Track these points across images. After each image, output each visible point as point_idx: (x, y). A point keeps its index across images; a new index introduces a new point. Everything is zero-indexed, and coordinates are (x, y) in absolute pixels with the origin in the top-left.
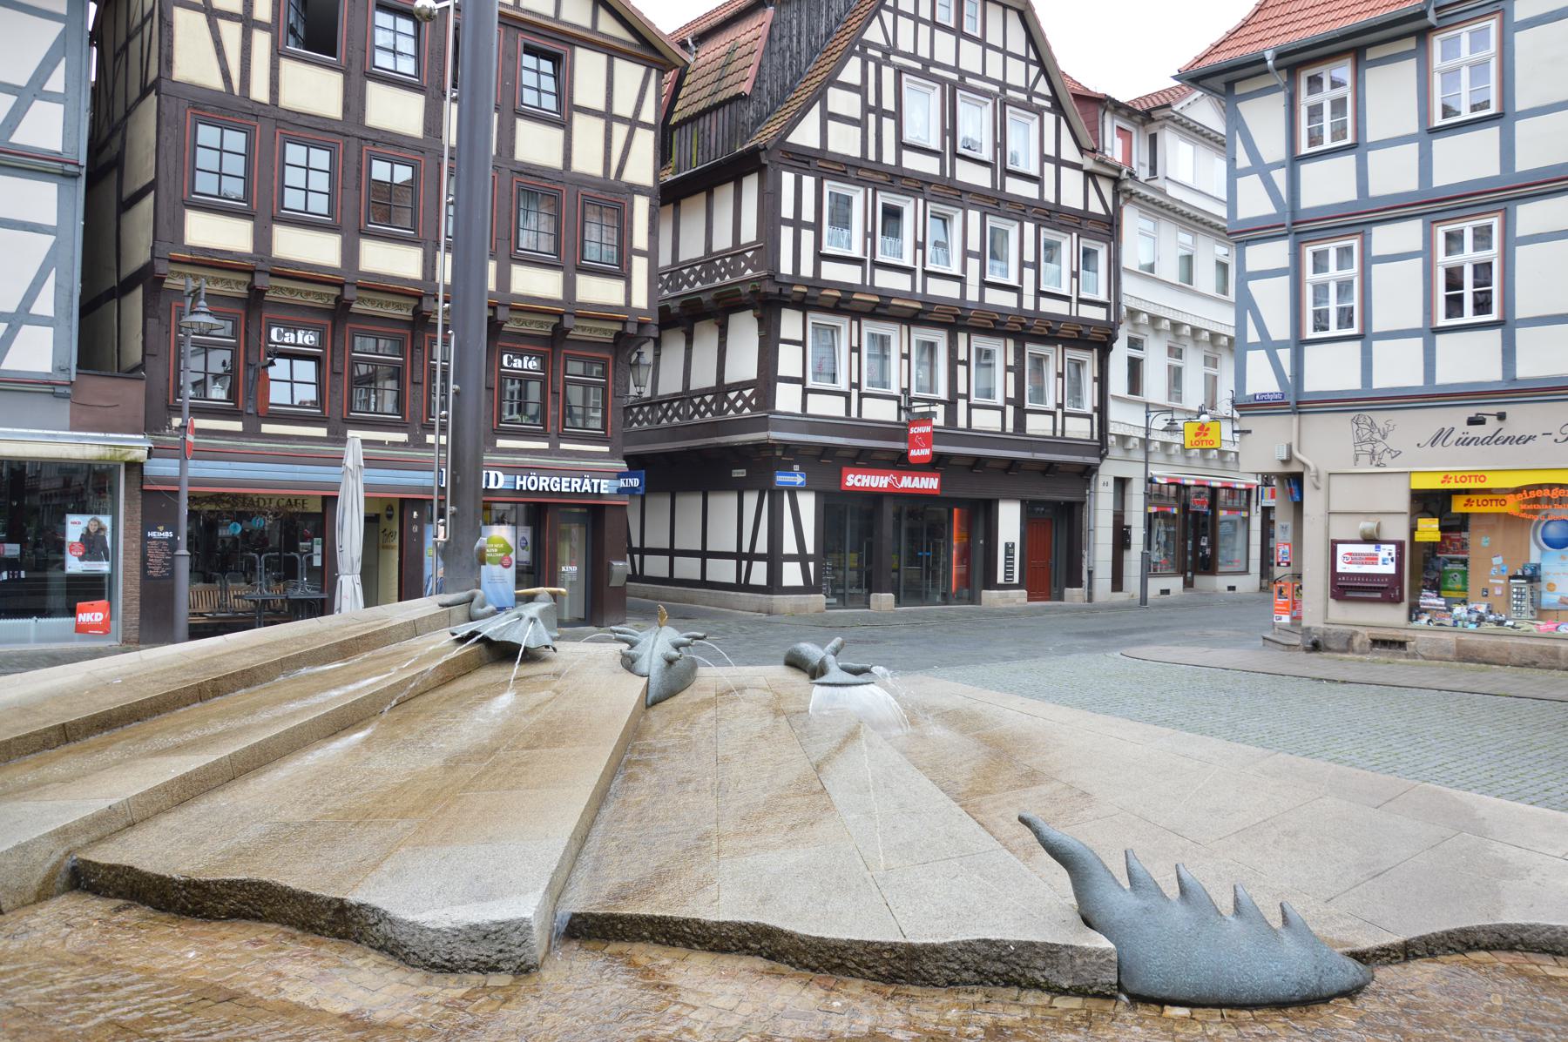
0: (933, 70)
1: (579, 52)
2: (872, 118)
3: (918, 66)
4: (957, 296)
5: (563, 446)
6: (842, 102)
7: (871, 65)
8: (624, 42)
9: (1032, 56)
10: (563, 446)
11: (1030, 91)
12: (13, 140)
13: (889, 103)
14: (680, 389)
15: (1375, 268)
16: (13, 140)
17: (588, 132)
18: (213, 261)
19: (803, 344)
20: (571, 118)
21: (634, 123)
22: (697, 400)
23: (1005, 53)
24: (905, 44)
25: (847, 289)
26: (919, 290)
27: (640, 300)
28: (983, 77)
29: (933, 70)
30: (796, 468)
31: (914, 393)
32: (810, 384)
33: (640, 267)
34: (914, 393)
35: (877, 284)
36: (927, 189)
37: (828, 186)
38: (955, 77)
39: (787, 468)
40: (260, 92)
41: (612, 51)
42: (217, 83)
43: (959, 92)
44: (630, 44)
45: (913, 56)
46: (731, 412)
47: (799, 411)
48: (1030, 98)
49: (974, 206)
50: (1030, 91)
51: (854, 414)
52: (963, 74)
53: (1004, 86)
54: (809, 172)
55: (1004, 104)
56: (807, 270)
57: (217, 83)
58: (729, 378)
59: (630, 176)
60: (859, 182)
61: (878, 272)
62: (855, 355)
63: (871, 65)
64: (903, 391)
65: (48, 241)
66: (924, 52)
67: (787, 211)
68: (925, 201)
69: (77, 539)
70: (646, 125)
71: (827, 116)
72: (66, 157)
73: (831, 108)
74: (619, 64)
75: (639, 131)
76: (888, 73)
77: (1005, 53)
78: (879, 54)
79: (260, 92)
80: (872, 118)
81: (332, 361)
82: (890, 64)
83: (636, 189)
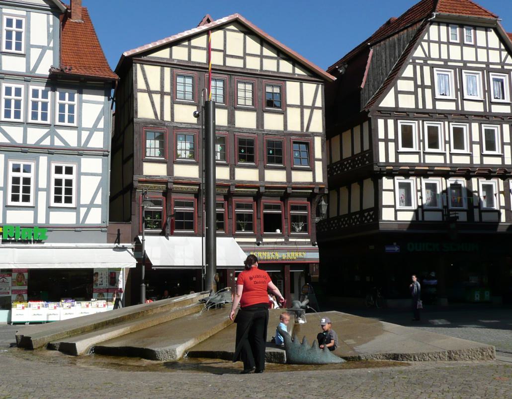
0: (449, 64)
1: (288, 83)
2: (420, 90)
3: (442, 63)
4: (468, 162)
5: (291, 240)
6: (402, 85)
7: (418, 67)
8: (303, 75)
9: (503, 47)
10: (291, 240)
11: (502, 64)
12: (88, 146)
13: (428, 82)
14: (336, 215)
15: (82, 177)
16: (88, 146)
17: (293, 115)
18: (154, 181)
19: (394, 190)
20: (286, 110)
21: (313, 108)
22: (353, 217)
23: (487, 48)
24: (434, 54)
25: (412, 165)
26: (448, 162)
27: (320, 178)
28: (477, 62)
29: (449, 64)
30: (395, 244)
31: (450, 207)
32: (398, 207)
33: (319, 166)
34: (450, 207)
35: (426, 162)
36: (449, 116)
37: (484, 127)
38: (461, 64)
39: (391, 245)
40: (167, 117)
41: (301, 80)
42: (152, 116)
43: (463, 71)
44: (305, 75)
45: (440, 59)
46: (366, 222)
47: (394, 220)
48: (503, 67)
49: (475, 121)
50: (502, 64)
51: (420, 219)
52: (465, 62)
53: (488, 64)
54: (390, 117)
55: (488, 72)
56: (392, 159)
57: (152, 116)
58: (365, 207)
59: (312, 130)
60: (414, 119)
61: (426, 156)
62: (419, 194)
63: (418, 67)
64: (444, 207)
65: (100, 178)
66: (444, 56)
67: (381, 135)
68: (449, 122)
69: (459, 183)
70: (318, 108)
71: (397, 93)
72: (104, 149)
73: (399, 89)
74: (305, 85)
75: (315, 111)
76: (427, 69)
77: (487, 48)
78: (422, 62)
79: (167, 117)
80: (420, 90)
81: (198, 212)
82: (428, 65)
83: (315, 134)
